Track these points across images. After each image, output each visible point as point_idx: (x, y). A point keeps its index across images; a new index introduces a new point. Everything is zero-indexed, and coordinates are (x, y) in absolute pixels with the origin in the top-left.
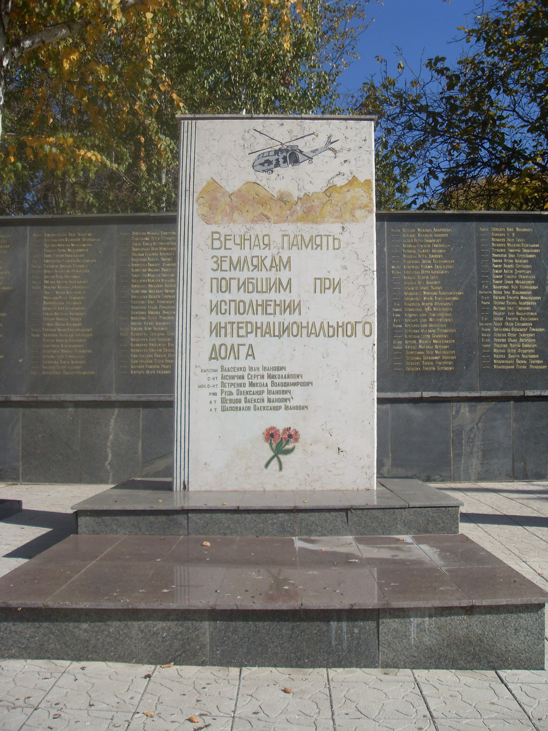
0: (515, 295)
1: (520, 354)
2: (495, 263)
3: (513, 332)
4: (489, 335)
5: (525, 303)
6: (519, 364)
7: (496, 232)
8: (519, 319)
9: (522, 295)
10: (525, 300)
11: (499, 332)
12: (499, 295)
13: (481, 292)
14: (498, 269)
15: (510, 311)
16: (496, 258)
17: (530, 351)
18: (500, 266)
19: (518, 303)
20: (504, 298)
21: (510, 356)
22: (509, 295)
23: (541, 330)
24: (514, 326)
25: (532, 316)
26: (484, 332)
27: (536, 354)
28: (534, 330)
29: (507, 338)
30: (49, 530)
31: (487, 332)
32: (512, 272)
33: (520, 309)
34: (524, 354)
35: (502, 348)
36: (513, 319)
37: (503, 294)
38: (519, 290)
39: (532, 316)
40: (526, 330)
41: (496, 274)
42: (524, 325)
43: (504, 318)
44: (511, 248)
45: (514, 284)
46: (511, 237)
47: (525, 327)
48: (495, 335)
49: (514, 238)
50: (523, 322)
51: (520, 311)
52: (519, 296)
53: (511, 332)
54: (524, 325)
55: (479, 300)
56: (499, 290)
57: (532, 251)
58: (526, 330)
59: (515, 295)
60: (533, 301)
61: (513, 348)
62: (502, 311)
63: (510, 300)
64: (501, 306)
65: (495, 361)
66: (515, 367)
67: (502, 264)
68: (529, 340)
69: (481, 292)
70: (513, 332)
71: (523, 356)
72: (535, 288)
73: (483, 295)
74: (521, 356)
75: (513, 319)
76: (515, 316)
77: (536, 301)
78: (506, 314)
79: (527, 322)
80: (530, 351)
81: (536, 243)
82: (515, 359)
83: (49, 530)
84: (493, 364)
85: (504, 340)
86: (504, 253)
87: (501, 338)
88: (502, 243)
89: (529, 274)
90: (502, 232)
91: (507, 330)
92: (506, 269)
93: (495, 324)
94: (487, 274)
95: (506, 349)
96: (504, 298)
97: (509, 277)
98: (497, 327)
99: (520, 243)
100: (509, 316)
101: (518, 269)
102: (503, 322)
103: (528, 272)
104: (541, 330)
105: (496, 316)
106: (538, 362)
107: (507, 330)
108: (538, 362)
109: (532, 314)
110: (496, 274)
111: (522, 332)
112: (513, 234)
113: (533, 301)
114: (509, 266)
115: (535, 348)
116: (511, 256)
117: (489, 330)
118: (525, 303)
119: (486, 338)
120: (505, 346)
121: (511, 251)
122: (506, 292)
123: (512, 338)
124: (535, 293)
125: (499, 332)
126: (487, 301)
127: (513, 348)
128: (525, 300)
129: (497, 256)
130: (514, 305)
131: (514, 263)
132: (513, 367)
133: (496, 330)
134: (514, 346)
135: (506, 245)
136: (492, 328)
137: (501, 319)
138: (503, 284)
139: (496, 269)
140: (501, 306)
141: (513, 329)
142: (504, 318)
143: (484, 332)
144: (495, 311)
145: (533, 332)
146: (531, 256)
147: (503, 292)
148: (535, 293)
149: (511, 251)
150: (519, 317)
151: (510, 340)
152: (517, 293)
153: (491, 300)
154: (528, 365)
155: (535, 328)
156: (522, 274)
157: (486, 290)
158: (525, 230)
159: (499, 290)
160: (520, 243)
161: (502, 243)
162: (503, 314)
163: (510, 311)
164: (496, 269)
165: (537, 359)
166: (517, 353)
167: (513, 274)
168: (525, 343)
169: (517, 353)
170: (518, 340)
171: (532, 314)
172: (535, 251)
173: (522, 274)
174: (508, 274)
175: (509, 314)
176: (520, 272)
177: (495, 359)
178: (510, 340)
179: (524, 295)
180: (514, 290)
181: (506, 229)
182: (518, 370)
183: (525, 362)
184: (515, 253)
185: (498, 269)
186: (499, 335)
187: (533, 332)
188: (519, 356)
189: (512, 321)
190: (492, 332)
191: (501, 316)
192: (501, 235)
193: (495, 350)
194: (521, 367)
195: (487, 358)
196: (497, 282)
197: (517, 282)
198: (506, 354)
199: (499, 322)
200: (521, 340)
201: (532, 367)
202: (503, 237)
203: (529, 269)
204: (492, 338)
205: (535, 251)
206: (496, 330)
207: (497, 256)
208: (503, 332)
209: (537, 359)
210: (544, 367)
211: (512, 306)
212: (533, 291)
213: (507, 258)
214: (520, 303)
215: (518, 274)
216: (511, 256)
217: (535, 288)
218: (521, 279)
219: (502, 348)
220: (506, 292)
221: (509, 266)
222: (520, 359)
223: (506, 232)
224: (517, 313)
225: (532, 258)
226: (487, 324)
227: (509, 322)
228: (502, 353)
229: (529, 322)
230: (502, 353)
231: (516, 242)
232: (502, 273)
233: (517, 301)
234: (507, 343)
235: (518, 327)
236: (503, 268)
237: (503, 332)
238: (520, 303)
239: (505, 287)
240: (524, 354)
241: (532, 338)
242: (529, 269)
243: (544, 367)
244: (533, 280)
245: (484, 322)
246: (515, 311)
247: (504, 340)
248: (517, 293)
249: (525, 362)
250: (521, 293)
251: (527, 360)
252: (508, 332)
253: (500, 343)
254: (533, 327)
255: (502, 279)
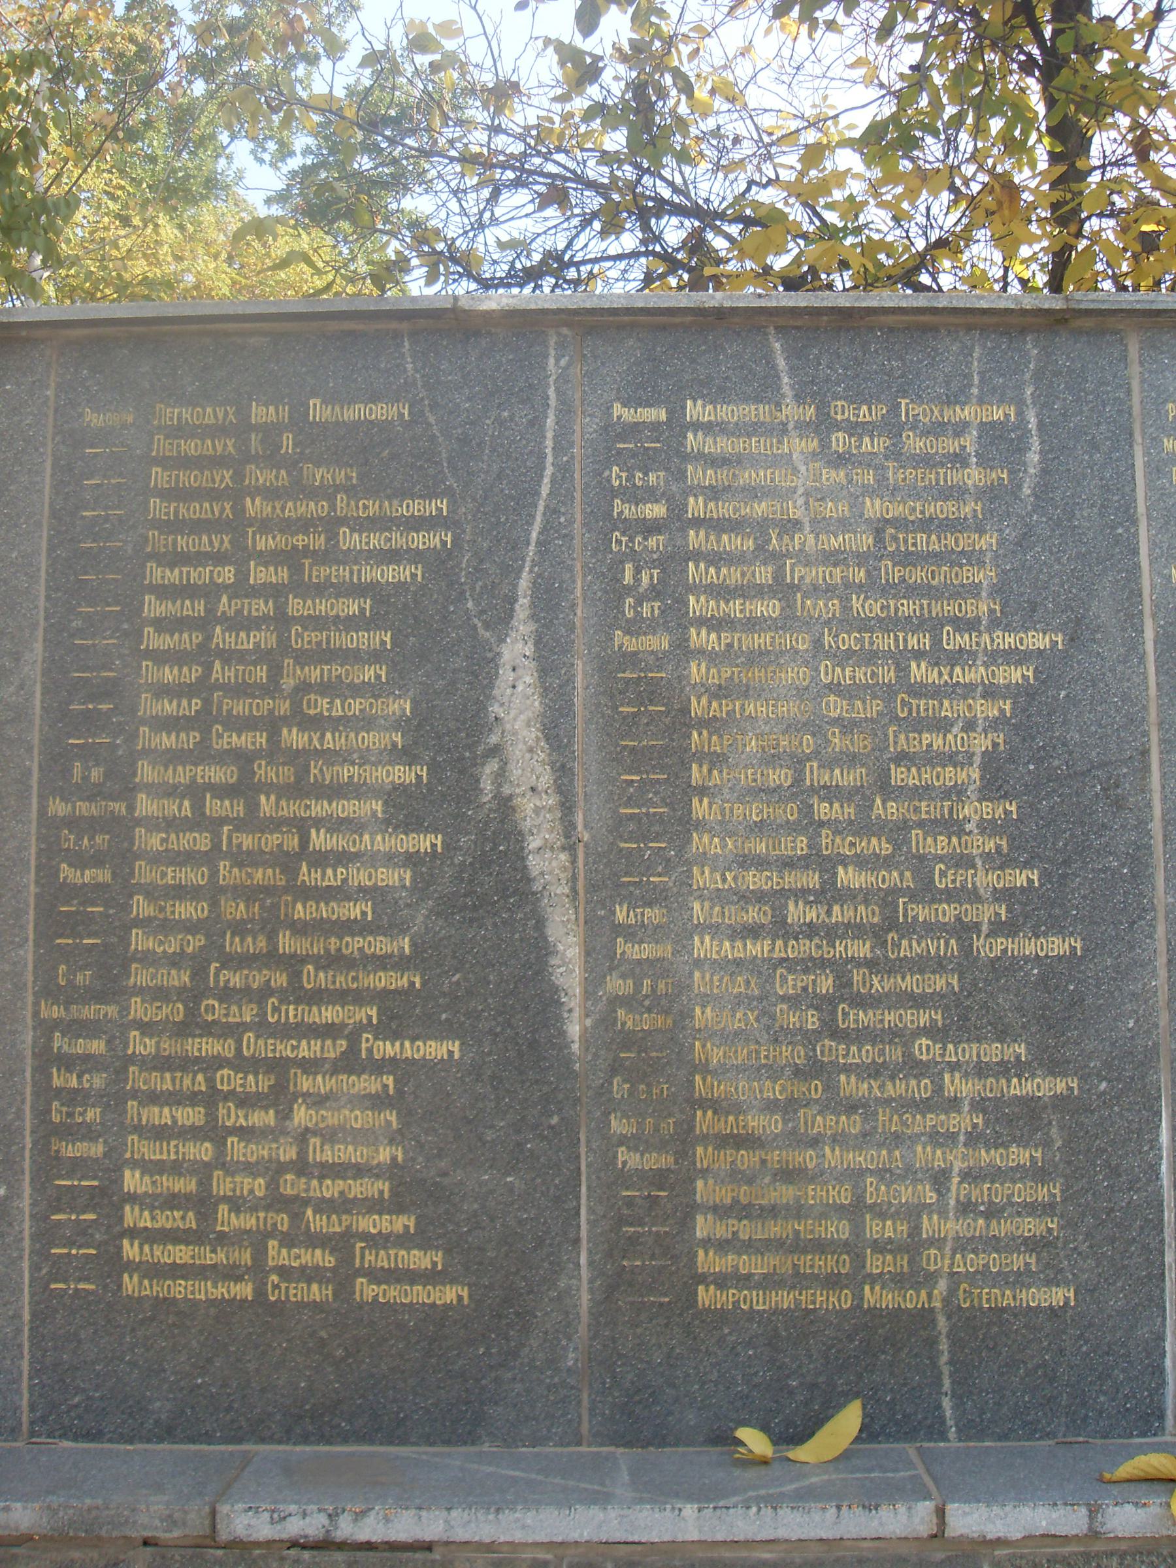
0: (275, 824)
1: (294, 1206)
2: (161, 625)
3: (252, 1065)
4: (98, 1081)
5: (331, 877)
6: (285, 1272)
7: (179, 431)
8: (295, 976)
9: (318, 823)
10: (343, 858)
11: (162, 1063)
12: (171, 824)
13: (58, 808)
14: (178, 658)
15: (239, 929)
16: (165, 592)
17: (358, 1188)
18: (189, 640)
19: (290, 870)
20: (203, 842)
21: (227, 1220)
22: (240, 825)
23: (435, 1050)
24: (262, 1027)
25: (382, 962)
26: (68, 1063)
27: (397, 1207)
28: (388, 1049)
29: (211, 1098)
30: (797, 8)
31: (87, 1063)
32: (261, 673)
33: (300, 911)
34: (326, 1206)
35: (176, 1168)
36: (257, 979)
37: (199, 821)
38: (299, 789)
39: (382, 962)
40: (334, 1049)
41: (163, 691)
42: (329, 1014)
43: (200, 973)
44: (265, 526)
45: (275, 752)
46: (272, 458)
47: (329, 1031)
48: (137, 1079)
49: (292, 465)
50: (318, 997)
51: (301, 929)
52: (302, 827)
53: (241, 1064)
54: (329, 1014)
55: (51, 852)
56: (172, 791)
57: (398, 540)
58: (334, 1049)
59: (275, 824)
60: (390, 859)
61: (250, 1169)
62: (191, 927)
63: (242, 859)
64: (180, 892)
65: (131, 1250)
66: (260, 1292)
67: (204, 624)
68: (359, 1118)
69: (58, 808)
70: (252, 1065)
71: (317, 1222)
72: (403, 774)
73: (71, 822)
74: (297, 1217)
75: (257, 979)
76: (272, 959)
77: (411, 860)
78: (214, 950)
79: (342, 997)
80: (358, 1188)
81: (430, 494)
82: (258, 1240)
83: (797, 8)
84: (114, 1265)
85: (191, 1116)
86: (220, 559)
87: (174, 1099)
88: (213, 495)
89: (374, 690)
90: (218, 431)
91: (210, 1047)
92: (228, 657)
93: (138, 1008)
94: (108, 690)
95: (203, 1171)
96: (203, 842)
97: (240, 707)
98: (146, 1028)
99: (327, 493)
100: (230, 961)
101: (304, 658)
102: (193, 996)
103: (369, 673)
104: (435, 1050)
105: (147, 959)
106: (419, 1259)
107: (210, 1047)
108: (419, 1259)
109: (380, 945)
110: (163, 691)
111: (310, 1066)
112: (288, 442)
113: (390, 859)
114: (248, 641)
115: (392, 1170)
116: (259, 574)
117: (97, 1046)
118: (331, 877)
119: (74, 1097)
120: (204, 1151)
121: (265, 543)
122: (215, 807)
123: (246, 1101)
124: (405, 810)
125: (162, 1063)
126: (97, 860)
127: (250, 1169)
128: (343, 858)
129: (173, 576)
130: (268, 890)
131: (282, 620)
132: (244, 1290)
133: (141, 1045)
134: (258, 1151)
135: (239, 510)
136: (116, 1033)
137: (181, 978)
138: (203, 754)
139: (161, 658)
140: (180, 892)
141: (252, 1045)
142: (200, 973)
143: (68, 1063)
144: (143, 923)
145: (379, 1067)
146: (390, 574)
147: (199, 806)
148: (405, 810)
149: (265, 543)
150: (293, 964)
151: (231, 1115)
152: (291, 809)
153: (122, 857)
154: (342, 1279)
155: (396, 1036)
156: (328, 688)
157: (94, 794)
158: (354, 413)
159: (172, 791)
160: (327, 493)
161: (213, 495)
162: (195, 943)
163: (239, 929)
164: (161, 658)
165: (404, 1240)
166: (276, 1201)
167: (271, 689)
168: (330, 1136)
169: (276, 1201)
170: (285, 1115)
171: (380, 945)
172: (419, 540)
173: (328, 688)
174: (241, 690)
175: (234, 945)
176: (314, 674)
177: (133, 1233)
178: (231, 1115)
179: (337, 825)
180: (268, 788)
181: (243, 412)
182: (278, 1309)
183: (323, 1258)
184: (290, 558)
185: (178, 658)
186: (165, 1082)
187: (379, 1067)
188: (283, 1221)
189: (246, 993)
190: (119, 1064)
191: (175, 960)
192: (208, 447)
193: (132, 1181)
194: (299, 1292)
195: (82, 1232)
196: (167, 741)
197: (294, 738)
198: (204, 1204)
199: (160, 994)
200: (302, 1115)
201: (366, 1290)
202: (218, 462)
203: (375, 657)
204: (114, 1099)
205: (419, 540)
206: (141, 1045)
207: (173, 576)
208: (186, 1064)
209: (404, 1240)
210: (449, 1294)
211: (249, 893)
212: (395, 796)
213: (241, 588)
214: (307, 875)
215: (304, 687)
216: (259, 574)
217: (403, 774)
218: (316, 723)
219: (176, 1168)
220: (215, 807)
221: (248, 641)
222: (288, 1241)
223: (242, 429)
224: (286, 943)
225: (401, 586)
226: (89, 1012)
227: (226, 995)
228: (172, 1201)
229: (358, 997)
230: (172, 1201)
231: (301, 490)
232: (202, 687)
233: (287, 862)
234: (214, 1132)
235: (286, 1031)
236: (204, 654)
237: (186, 1064)
238: (307, 875)
239: (217, 774)
240: (326, 1206)
241: (377, 1102)
242: (375, 657)
243: (449, 1294)
244: (398, 724)
245: (70, 996)
246: (270, 925)
247: (191, 1116)
248: (291, 809)
249: (323, 1258)
250: (319, 808)
251: (341, 1244)
252: (219, 1062)
253: (160, 1133)
254: (388, 1028)
255: (202, 721)
